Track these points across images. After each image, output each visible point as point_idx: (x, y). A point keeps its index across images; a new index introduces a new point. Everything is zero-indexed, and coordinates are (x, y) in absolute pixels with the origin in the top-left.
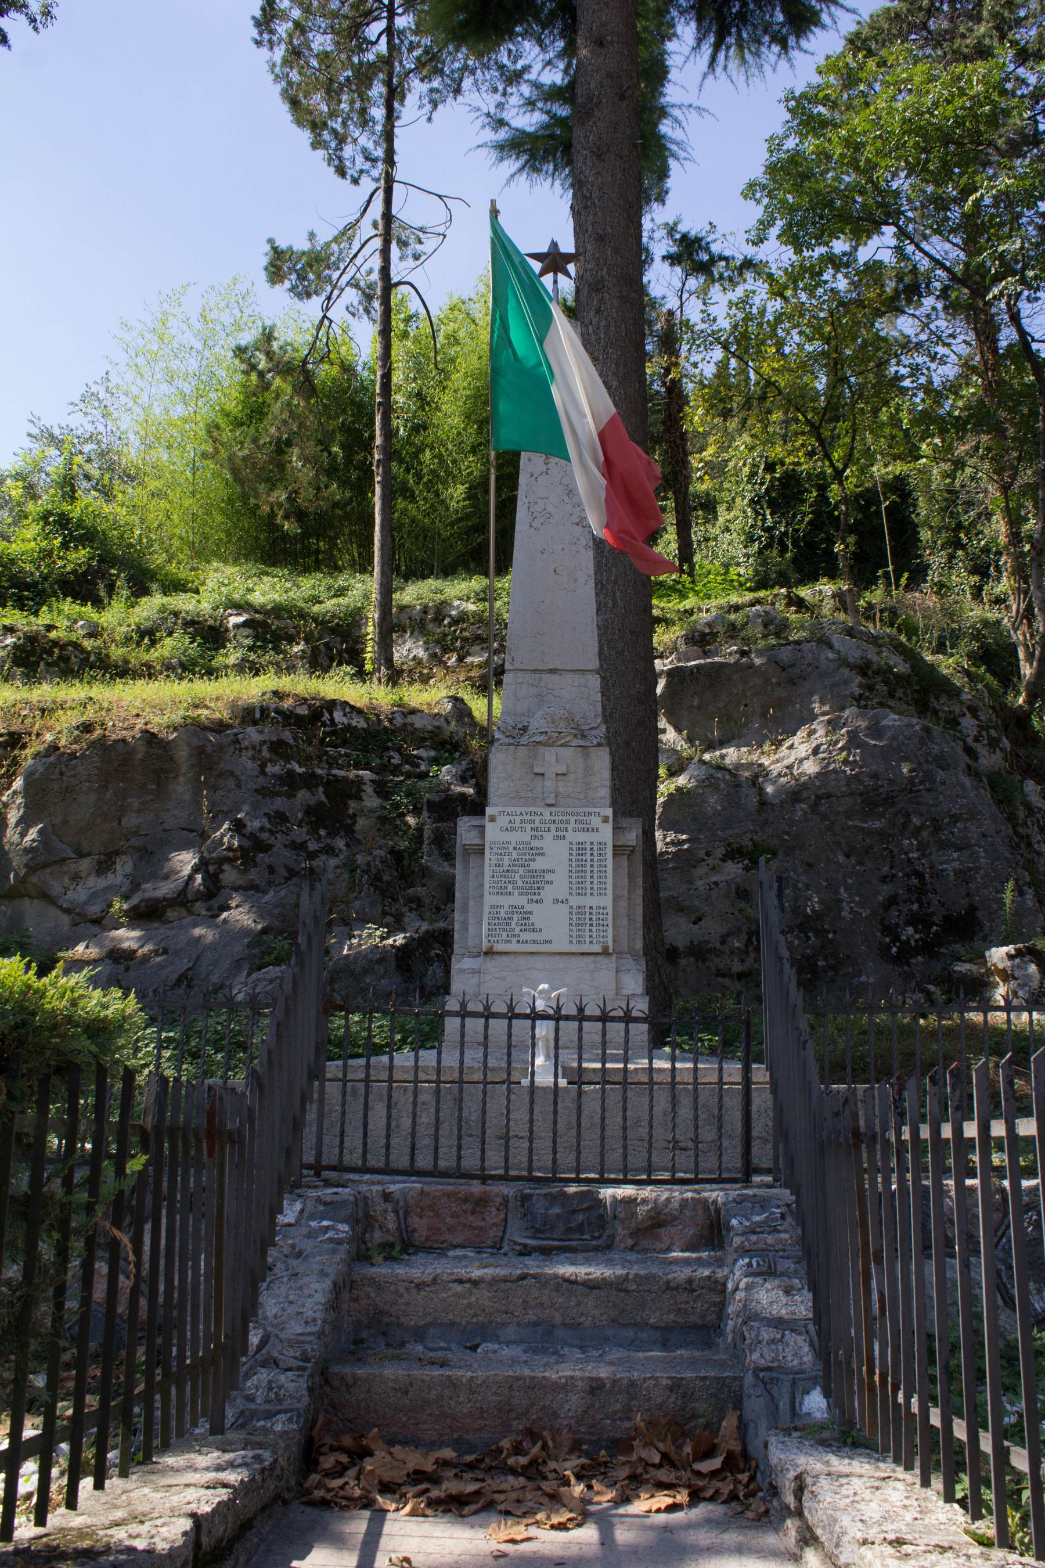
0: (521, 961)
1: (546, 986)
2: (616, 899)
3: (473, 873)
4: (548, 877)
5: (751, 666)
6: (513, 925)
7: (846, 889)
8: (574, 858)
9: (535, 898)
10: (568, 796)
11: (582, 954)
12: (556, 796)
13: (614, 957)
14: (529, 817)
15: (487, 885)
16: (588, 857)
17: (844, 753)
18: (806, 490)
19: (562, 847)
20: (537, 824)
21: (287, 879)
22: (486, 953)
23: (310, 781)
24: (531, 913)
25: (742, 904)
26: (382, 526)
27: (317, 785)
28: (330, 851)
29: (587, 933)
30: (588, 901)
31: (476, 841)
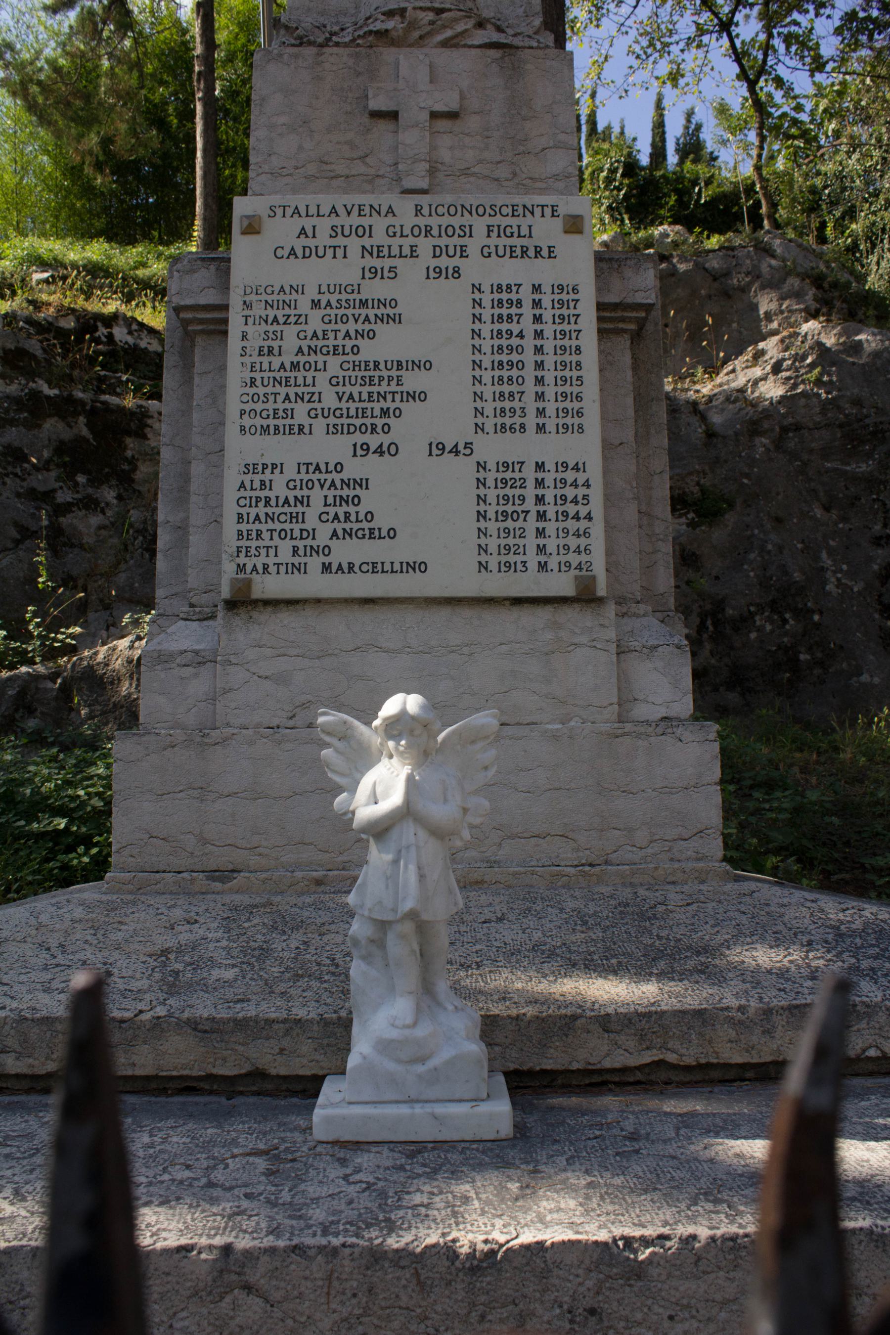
0: (337, 626)
1: (413, 703)
2: (608, 446)
3: (201, 388)
4: (412, 381)
6: (312, 521)
7: (829, 554)
8: (486, 329)
9: (374, 441)
10: (466, 172)
11: (517, 601)
12: (432, 172)
13: (611, 610)
14: (355, 220)
15: (233, 407)
17: (816, 371)
18: (665, 195)
19: (453, 299)
20: (380, 238)
21: (17, 542)
22: (232, 605)
23: (65, 408)
24: (363, 483)
26: (205, 150)
27: (76, 414)
28: (91, 504)
29: (531, 542)
30: (529, 448)
31: (210, 297)
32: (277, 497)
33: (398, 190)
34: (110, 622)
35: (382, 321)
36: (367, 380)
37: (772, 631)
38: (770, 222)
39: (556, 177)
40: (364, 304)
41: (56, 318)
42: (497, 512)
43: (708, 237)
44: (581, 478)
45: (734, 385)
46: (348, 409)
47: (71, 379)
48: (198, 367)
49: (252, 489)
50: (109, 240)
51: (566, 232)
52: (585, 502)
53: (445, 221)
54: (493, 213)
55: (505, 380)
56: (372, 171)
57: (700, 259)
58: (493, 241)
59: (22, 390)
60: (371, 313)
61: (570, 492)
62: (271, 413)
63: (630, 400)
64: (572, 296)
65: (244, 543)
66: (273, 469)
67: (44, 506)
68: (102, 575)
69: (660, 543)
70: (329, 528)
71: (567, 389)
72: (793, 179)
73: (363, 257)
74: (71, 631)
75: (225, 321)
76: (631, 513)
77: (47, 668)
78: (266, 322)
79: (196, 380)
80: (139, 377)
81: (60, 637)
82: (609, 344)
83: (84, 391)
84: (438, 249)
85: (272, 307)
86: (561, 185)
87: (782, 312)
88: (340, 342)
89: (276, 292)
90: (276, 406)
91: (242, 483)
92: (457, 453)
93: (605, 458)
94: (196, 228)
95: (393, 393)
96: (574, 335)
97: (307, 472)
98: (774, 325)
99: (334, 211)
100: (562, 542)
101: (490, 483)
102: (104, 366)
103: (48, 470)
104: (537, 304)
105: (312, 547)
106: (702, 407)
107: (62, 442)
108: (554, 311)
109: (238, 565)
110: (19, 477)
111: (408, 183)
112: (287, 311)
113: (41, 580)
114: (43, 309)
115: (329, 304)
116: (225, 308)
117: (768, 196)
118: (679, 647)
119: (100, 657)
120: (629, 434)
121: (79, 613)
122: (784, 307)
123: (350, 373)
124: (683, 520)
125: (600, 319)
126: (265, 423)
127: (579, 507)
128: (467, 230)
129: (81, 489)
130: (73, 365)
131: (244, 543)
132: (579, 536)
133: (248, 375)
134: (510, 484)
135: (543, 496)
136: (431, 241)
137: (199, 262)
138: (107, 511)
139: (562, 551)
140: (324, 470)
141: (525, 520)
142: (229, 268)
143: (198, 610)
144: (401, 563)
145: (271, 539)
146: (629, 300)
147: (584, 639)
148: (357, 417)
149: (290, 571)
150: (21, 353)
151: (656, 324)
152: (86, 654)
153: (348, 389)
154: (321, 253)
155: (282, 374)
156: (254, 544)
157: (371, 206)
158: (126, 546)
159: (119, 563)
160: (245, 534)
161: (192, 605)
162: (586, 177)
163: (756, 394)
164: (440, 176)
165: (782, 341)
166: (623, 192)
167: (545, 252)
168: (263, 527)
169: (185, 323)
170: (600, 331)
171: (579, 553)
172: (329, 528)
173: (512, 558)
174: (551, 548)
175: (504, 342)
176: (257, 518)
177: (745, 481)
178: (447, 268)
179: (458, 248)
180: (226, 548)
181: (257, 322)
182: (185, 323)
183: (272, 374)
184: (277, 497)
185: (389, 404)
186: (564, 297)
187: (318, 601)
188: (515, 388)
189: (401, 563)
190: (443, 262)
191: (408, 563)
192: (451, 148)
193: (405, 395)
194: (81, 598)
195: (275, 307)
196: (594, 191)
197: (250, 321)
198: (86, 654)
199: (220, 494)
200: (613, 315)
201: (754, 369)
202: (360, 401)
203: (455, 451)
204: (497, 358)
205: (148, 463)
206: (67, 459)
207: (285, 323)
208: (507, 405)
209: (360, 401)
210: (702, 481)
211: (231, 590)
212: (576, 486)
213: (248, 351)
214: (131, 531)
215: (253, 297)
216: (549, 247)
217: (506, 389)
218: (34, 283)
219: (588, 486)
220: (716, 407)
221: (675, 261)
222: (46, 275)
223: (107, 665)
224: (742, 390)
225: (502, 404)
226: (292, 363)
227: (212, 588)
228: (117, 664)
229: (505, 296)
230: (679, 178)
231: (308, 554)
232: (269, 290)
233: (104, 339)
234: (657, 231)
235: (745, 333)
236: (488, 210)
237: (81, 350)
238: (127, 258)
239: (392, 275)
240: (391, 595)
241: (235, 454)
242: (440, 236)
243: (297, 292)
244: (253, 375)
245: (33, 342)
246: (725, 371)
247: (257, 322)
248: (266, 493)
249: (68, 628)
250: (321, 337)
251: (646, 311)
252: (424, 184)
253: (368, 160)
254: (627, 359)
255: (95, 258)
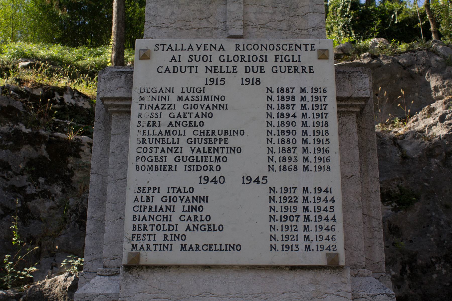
0: (188, 281)
2: (345, 178)
3: (114, 143)
4: (233, 141)
5: (380, 65)
6: (175, 220)
8: (275, 113)
9: (211, 175)
10: (263, 26)
11: (293, 268)
12: (245, 26)
13: (348, 273)
15: (132, 153)
16: (298, 111)
18: (375, 19)
20: (216, 62)
22: (128, 268)
23: (34, 140)
24: (205, 199)
25: (395, 239)
27: (40, 143)
28: (46, 195)
29: (301, 233)
30: (299, 179)
32: (156, 206)
33: (227, 36)
34: (54, 265)
35: (217, 108)
36: (208, 141)
37: (446, 274)
38: (435, 36)
39: (313, 28)
40: (206, 98)
41: (32, 89)
42: (281, 216)
43: (400, 44)
44: (329, 197)
45: (417, 128)
46: (197, 157)
47: (38, 123)
48: (113, 131)
49: (142, 201)
50: (63, 44)
51: (319, 59)
52: (332, 210)
53: (252, 53)
54: (278, 49)
55: (286, 141)
56: (212, 26)
57: (395, 57)
58: (278, 64)
59: (10, 129)
60: (211, 103)
61: (323, 205)
62: (154, 158)
63: (357, 151)
64: (323, 94)
65: (136, 232)
66: (154, 190)
67: (19, 195)
68: (50, 236)
69: (376, 232)
70: (185, 224)
71: (321, 146)
72: (448, 9)
73: (206, 73)
74: (30, 269)
75: (130, 106)
76: (358, 216)
77: (14, 292)
78: (152, 108)
79: (112, 138)
80: (77, 123)
81: (24, 273)
82: (344, 119)
83: (45, 130)
84: (248, 68)
85: (156, 99)
86: (316, 33)
87: (444, 86)
88: (193, 119)
89: (158, 91)
90: (156, 155)
91: (137, 198)
92: (258, 182)
93: (343, 184)
94: (112, 39)
95: (223, 148)
96: (324, 116)
97: (173, 192)
98: (440, 94)
99: (191, 47)
100: (318, 233)
101: (277, 199)
102: (57, 116)
103: (22, 175)
104: (303, 98)
105: (175, 235)
106: (399, 142)
107: (31, 159)
108: (313, 103)
109: (133, 245)
110: (5, 179)
111: (232, 32)
112: (164, 102)
113: (14, 239)
114: (25, 84)
115: (187, 98)
116: (130, 99)
117: (434, 20)
118: (389, 296)
119: (47, 286)
120: (356, 170)
121: (36, 258)
122: (445, 83)
123: (198, 137)
124: (390, 207)
125: (339, 106)
126: (150, 164)
127: (329, 213)
128: (264, 58)
129: (41, 186)
130: (40, 116)
131: (136, 232)
132: (328, 230)
133: (141, 137)
134: (288, 200)
135: (307, 207)
136: (244, 64)
137: (115, 74)
138: (55, 199)
139: (319, 239)
140: (183, 191)
141: (297, 221)
142: (132, 77)
143: (108, 270)
144: (226, 245)
145: (152, 230)
146: (355, 95)
147: (333, 291)
148: (202, 161)
149: (162, 249)
150: (11, 109)
151: (371, 107)
152: (38, 283)
153: (197, 146)
154: (183, 71)
155: (161, 136)
156: (142, 233)
157: (211, 45)
158: (65, 219)
159: (61, 229)
160: (137, 227)
161: (105, 267)
162: (330, 10)
163: (431, 134)
164: (249, 28)
165: (445, 103)
166: (350, 19)
167: (307, 70)
168: (148, 223)
169: (107, 107)
170: (339, 112)
171: (329, 240)
172: (185, 224)
173: (289, 243)
174: (312, 237)
175: (285, 120)
176: (144, 218)
177: (426, 184)
178: (253, 79)
179: (259, 68)
180: (126, 235)
181: (147, 108)
182: (107, 107)
183: (154, 137)
184: (156, 206)
185: (220, 154)
186: (318, 94)
187: (178, 266)
188: (291, 146)
189: (226, 245)
190: (251, 75)
191: (230, 245)
192: (255, 13)
193: (229, 149)
194: (37, 249)
195: (157, 99)
196: (334, 17)
197: (143, 107)
198: (38, 283)
199: (124, 203)
200: (346, 103)
201: (429, 119)
202: (204, 152)
203: (257, 181)
204: (281, 128)
205: (81, 171)
206: (34, 169)
207: (162, 109)
208: (287, 155)
209: (204, 152)
210: (400, 184)
211: (128, 260)
212: (327, 201)
213: (141, 124)
214: (69, 211)
215: (145, 94)
216: (310, 67)
217: (286, 146)
218: (19, 67)
219: (333, 201)
220: (407, 141)
221: (381, 58)
222: (27, 63)
223: (51, 291)
224: (422, 132)
225: (283, 137)
226: (166, 131)
227: (117, 257)
228: (57, 290)
229: (285, 94)
230: (383, 10)
231: (173, 239)
232: (154, 90)
233: (58, 101)
234: (370, 42)
235: (423, 98)
236: (276, 47)
237: (45, 107)
238: (73, 54)
239: (223, 82)
240: (220, 263)
241: (133, 178)
242: (249, 61)
243: (170, 91)
244: (144, 137)
245: (18, 102)
246: (412, 120)
247: (147, 108)
248: (150, 204)
249: (28, 268)
250: (182, 117)
251: (365, 101)
252: (240, 33)
253: (209, 19)
254: (355, 127)
255: (55, 54)
